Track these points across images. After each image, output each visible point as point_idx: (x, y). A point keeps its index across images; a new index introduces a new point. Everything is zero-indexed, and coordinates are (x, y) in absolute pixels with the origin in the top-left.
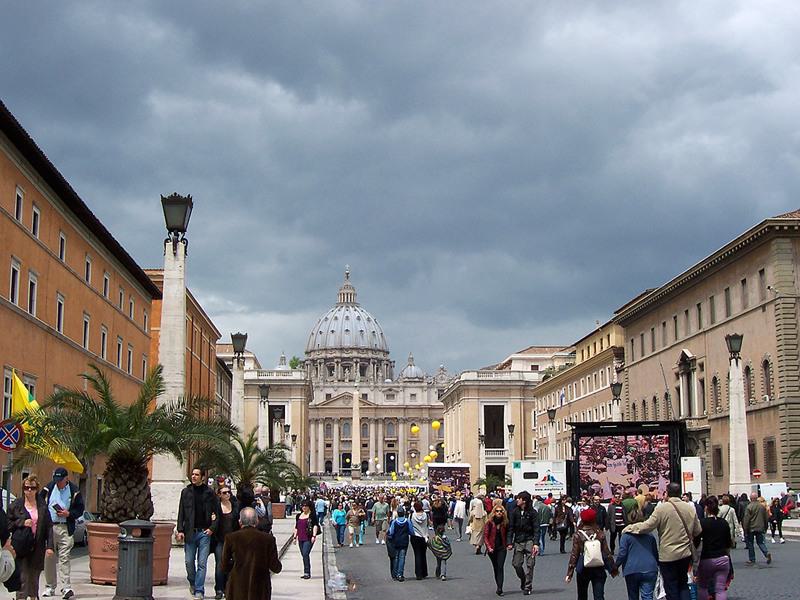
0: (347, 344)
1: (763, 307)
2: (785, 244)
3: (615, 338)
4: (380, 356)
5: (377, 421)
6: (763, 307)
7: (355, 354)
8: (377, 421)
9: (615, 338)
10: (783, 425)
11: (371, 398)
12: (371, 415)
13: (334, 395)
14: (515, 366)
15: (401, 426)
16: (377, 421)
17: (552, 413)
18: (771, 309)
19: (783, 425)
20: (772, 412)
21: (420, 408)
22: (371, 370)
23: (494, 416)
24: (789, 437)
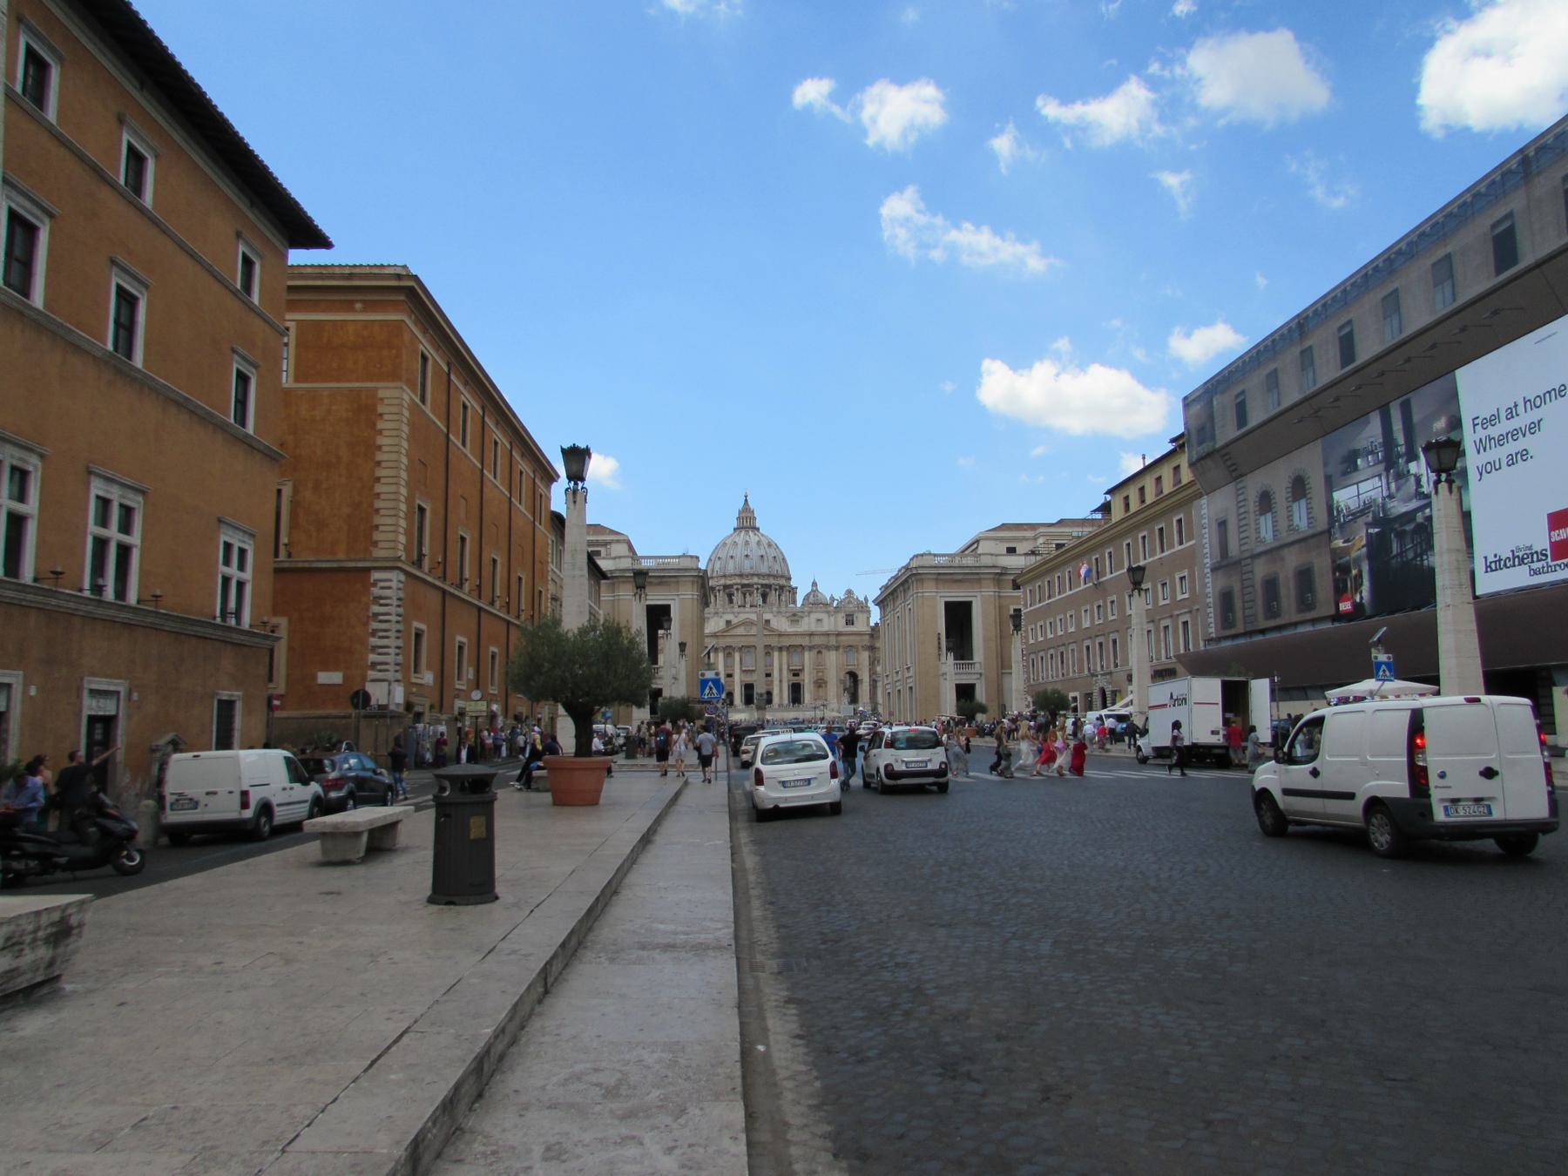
0: (747, 570)
4: (783, 582)
5: (780, 649)
7: (755, 580)
8: (780, 649)
11: (774, 624)
12: (774, 642)
13: (735, 621)
17: (1137, 576)
21: (827, 634)
22: (773, 597)
23: (958, 616)
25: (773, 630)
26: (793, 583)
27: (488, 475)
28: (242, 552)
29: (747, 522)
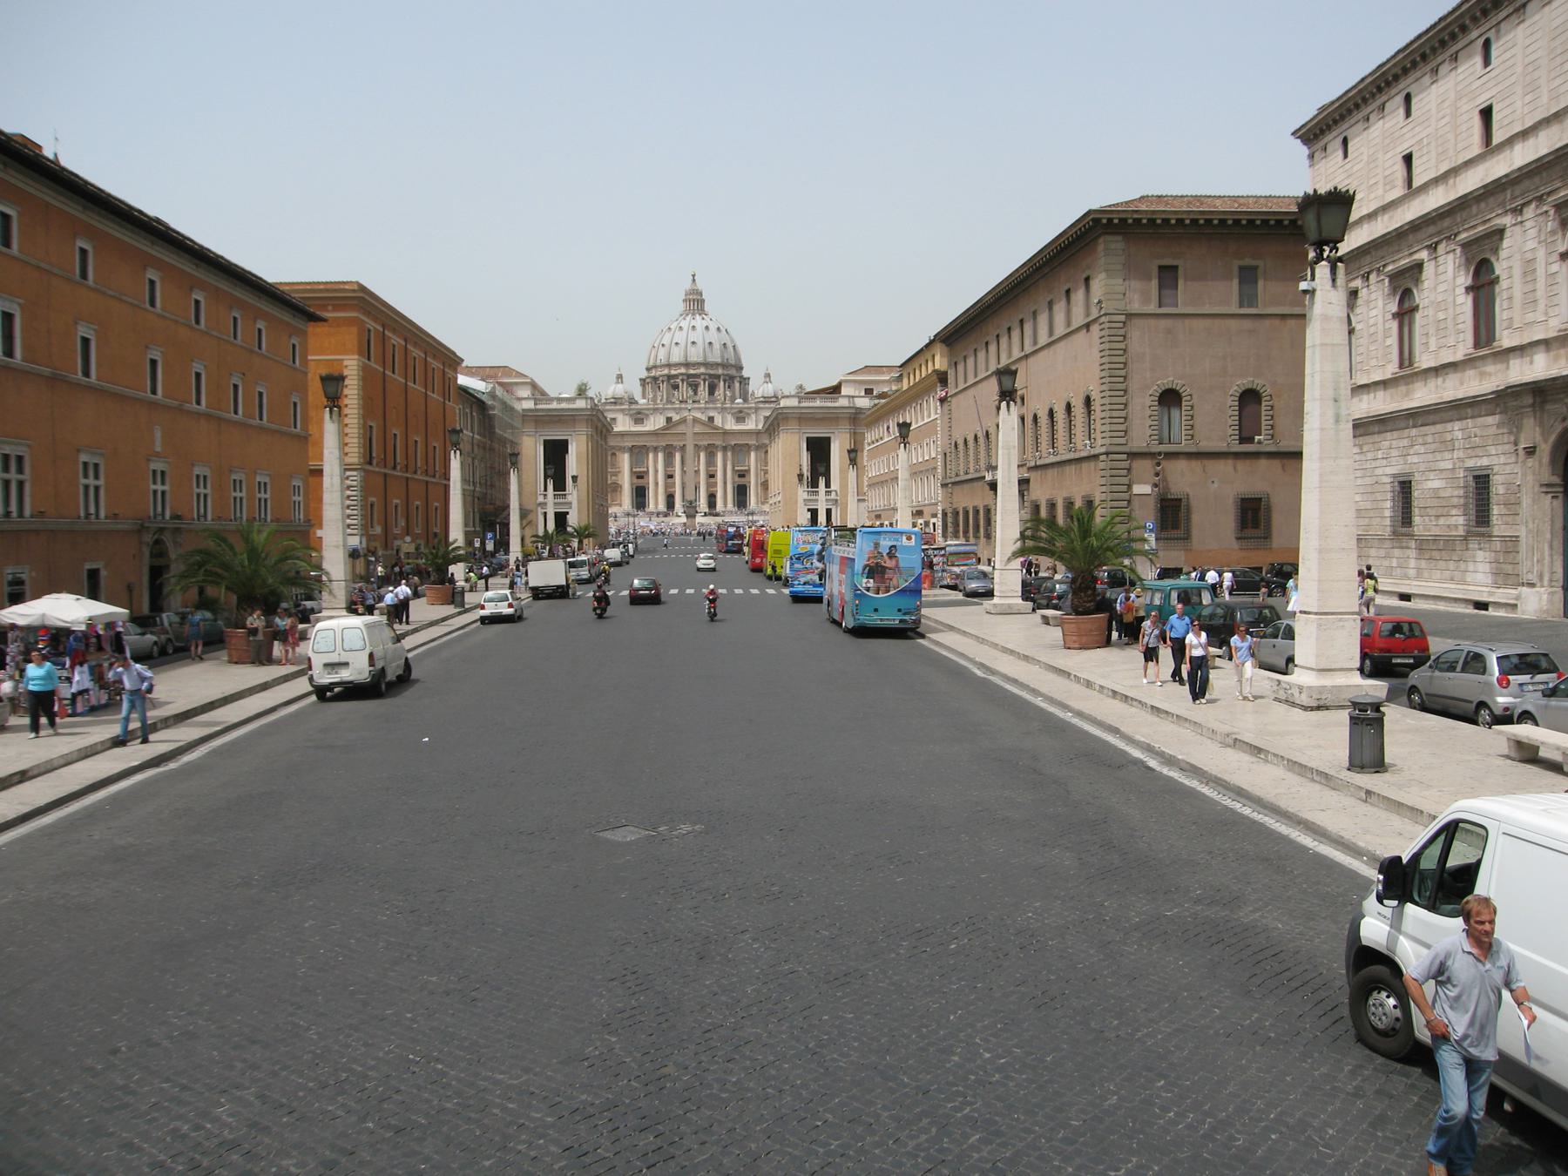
0: (693, 358)
1: (1087, 326)
2: (1115, 243)
3: (939, 362)
4: (733, 372)
6: (1087, 326)
9: (939, 362)
10: (1103, 481)
11: (718, 421)
13: (676, 417)
14: (845, 391)
15: (753, 454)
16: (725, 449)
18: (1095, 328)
19: (1103, 481)
20: (1092, 464)
24: (1110, 496)
25: (716, 428)
26: (745, 373)
27: (410, 384)
28: (96, 466)
29: (695, 303)
